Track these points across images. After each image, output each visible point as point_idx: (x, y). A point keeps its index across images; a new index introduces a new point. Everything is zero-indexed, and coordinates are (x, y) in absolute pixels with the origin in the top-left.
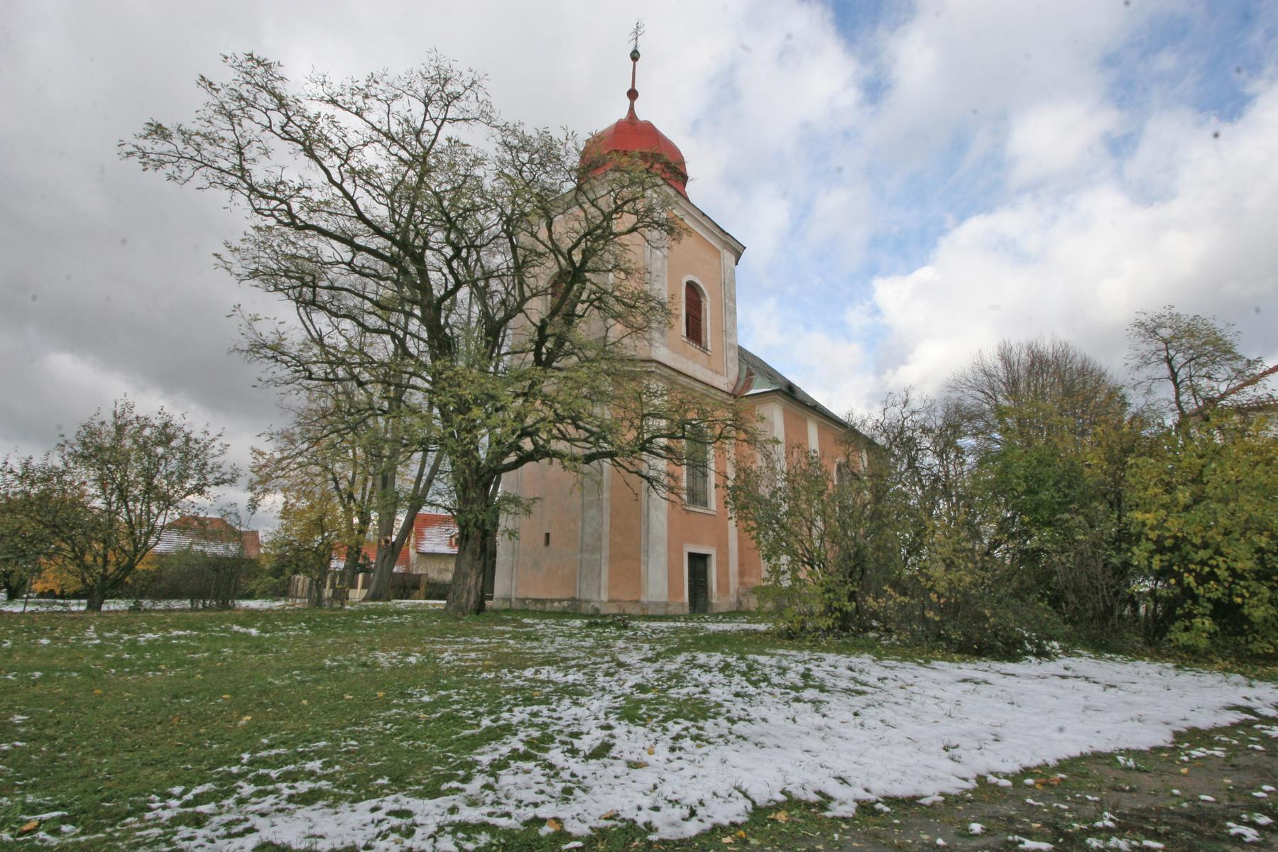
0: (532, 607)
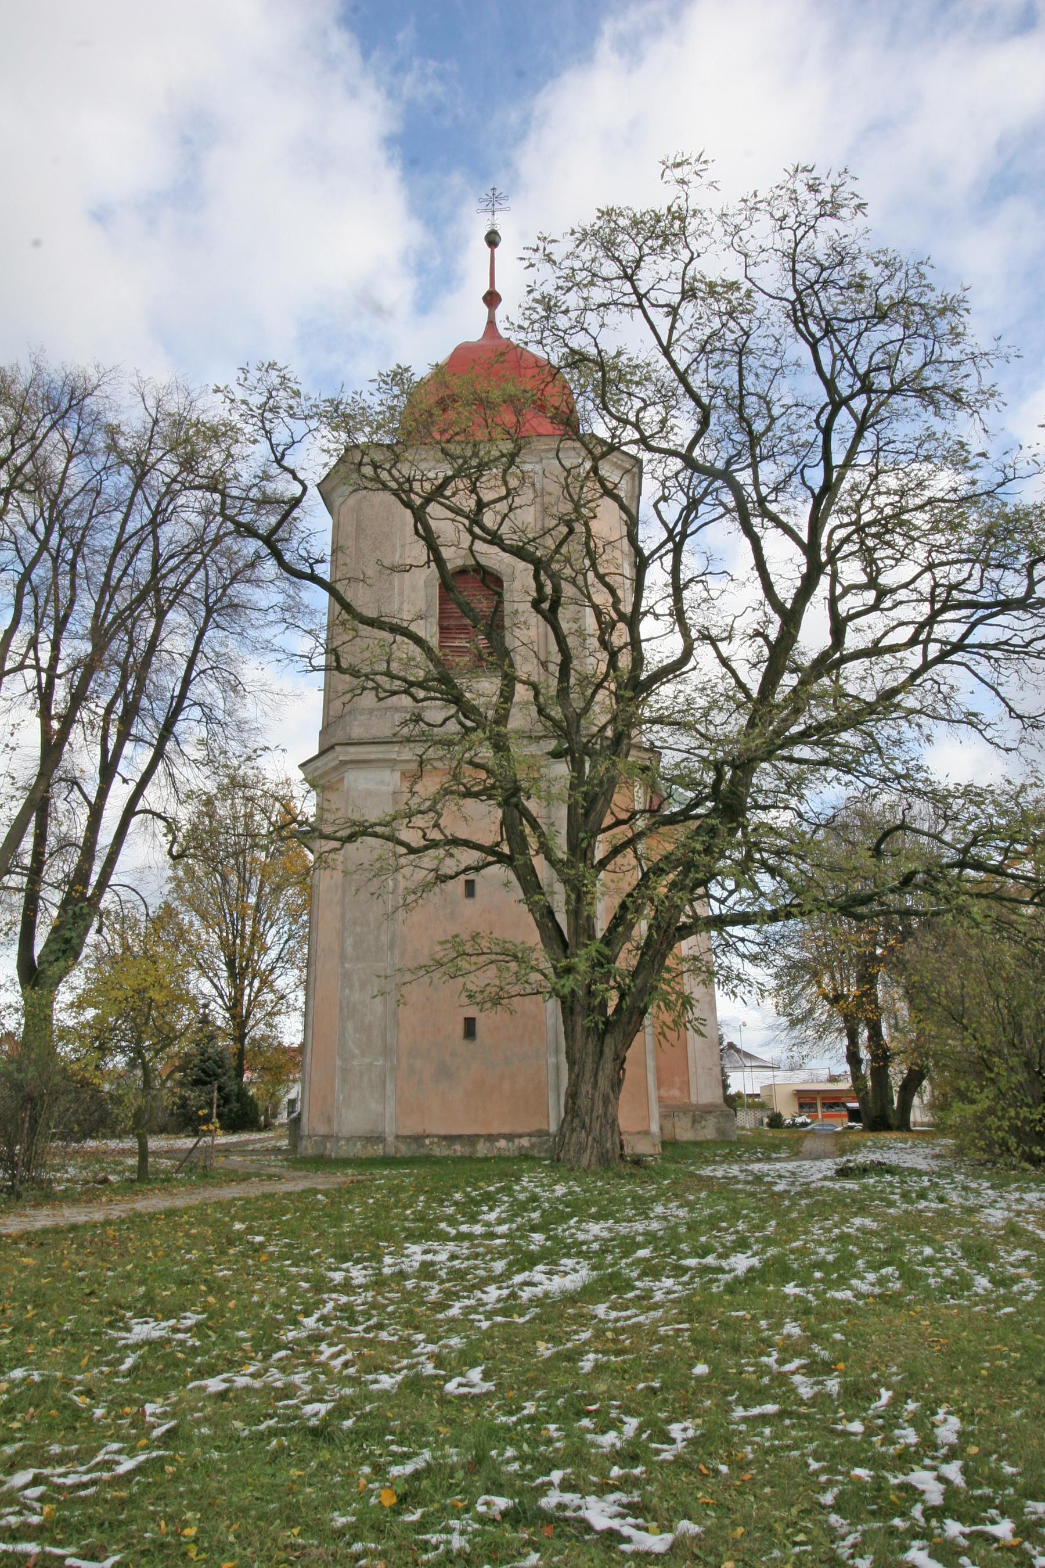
0: (440, 1151)
